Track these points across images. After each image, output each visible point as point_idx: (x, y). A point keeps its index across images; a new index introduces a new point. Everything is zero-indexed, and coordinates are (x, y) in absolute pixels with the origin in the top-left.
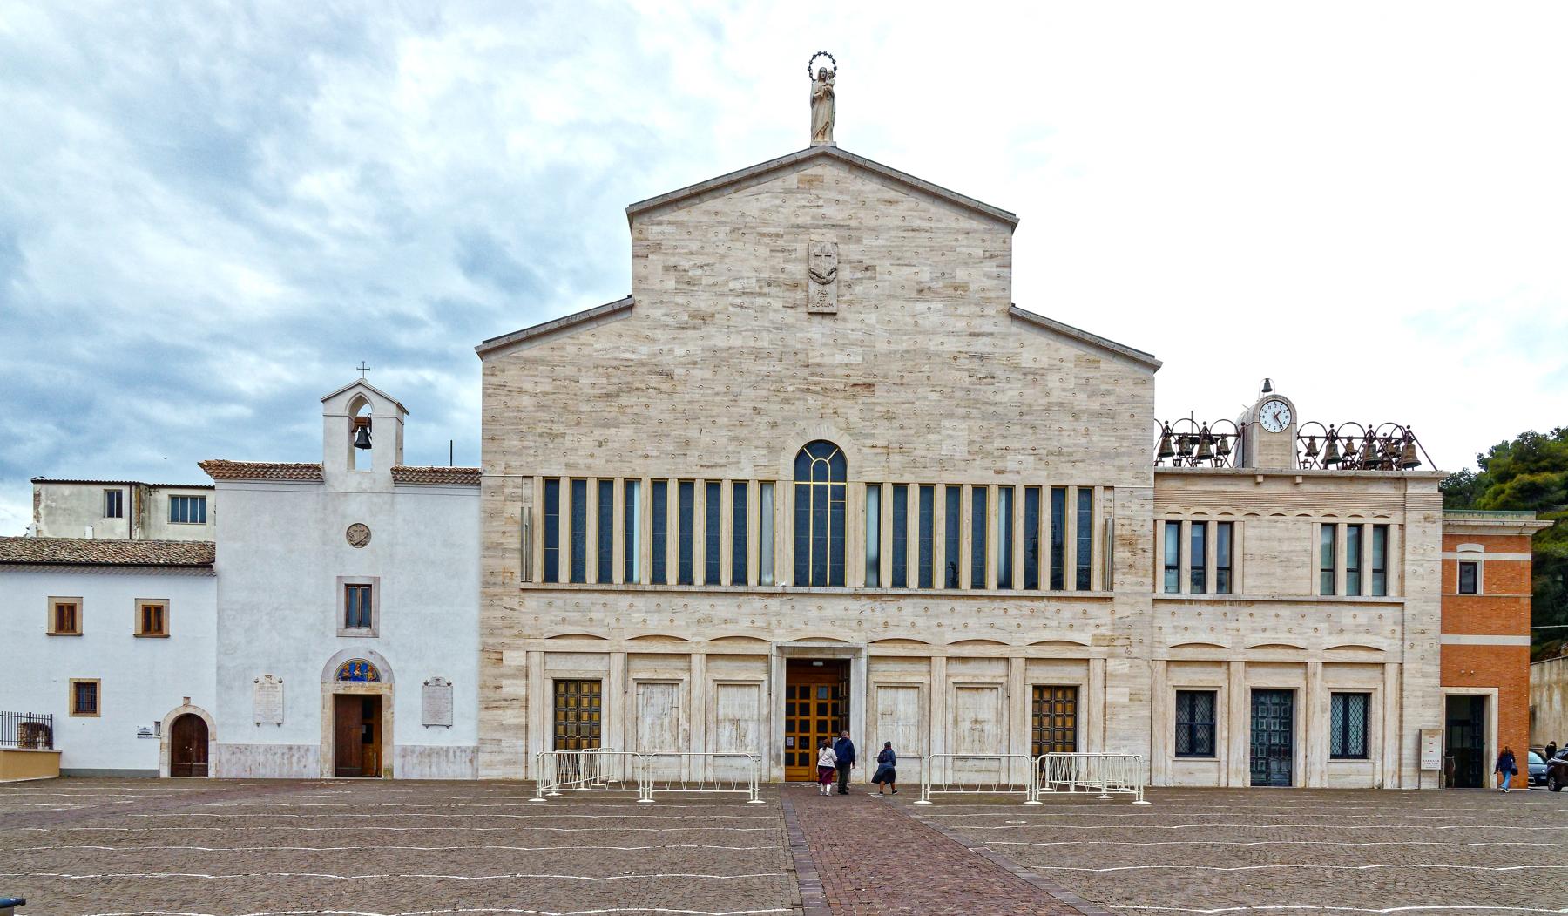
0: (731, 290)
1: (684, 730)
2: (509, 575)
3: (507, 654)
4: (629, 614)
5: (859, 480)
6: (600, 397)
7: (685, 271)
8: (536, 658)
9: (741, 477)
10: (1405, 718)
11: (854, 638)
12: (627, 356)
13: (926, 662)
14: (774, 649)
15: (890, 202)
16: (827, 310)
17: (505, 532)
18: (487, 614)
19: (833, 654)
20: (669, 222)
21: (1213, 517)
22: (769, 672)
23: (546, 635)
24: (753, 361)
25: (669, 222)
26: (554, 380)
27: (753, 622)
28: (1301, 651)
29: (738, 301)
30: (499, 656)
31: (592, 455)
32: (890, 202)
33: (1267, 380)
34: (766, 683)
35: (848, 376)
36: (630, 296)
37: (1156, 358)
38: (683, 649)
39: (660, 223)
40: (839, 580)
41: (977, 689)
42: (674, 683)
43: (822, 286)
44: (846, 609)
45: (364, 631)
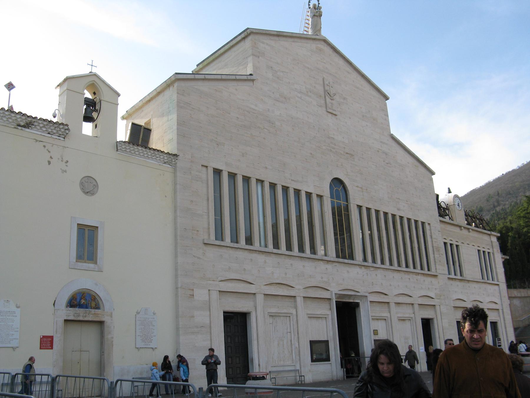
0: (295, 89)
1: (296, 348)
2: (196, 232)
3: (197, 292)
4: (264, 268)
5: (354, 203)
6: (241, 126)
7: (275, 71)
8: (215, 295)
9: (309, 191)
10: (508, 335)
11: (362, 290)
12: (253, 106)
13: (386, 305)
14: (334, 295)
15: (348, 72)
16: (334, 112)
17: (192, 201)
18: (518, 288)
19: (353, 300)
20: (267, 44)
21: (455, 243)
22: (296, 308)
23: (220, 279)
24: (308, 128)
25: (267, 44)
26: (217, 109)
27: (322, 278)
28: (220, 280)
29: (299, 95)
30: (191, 293)
31: (239, 161)
32: (348, 72)
33: (449, 188)
34: (330, 316)
35: (344, 148)
36: (251, 75)
37: (504, 174)
38: (292, 293)
39: (263, 43)
40: (351, 257)
41: (404, 320)
42: (288, 316)
43: (331, 100)
44: (358, 273)
45: (92, 266)
